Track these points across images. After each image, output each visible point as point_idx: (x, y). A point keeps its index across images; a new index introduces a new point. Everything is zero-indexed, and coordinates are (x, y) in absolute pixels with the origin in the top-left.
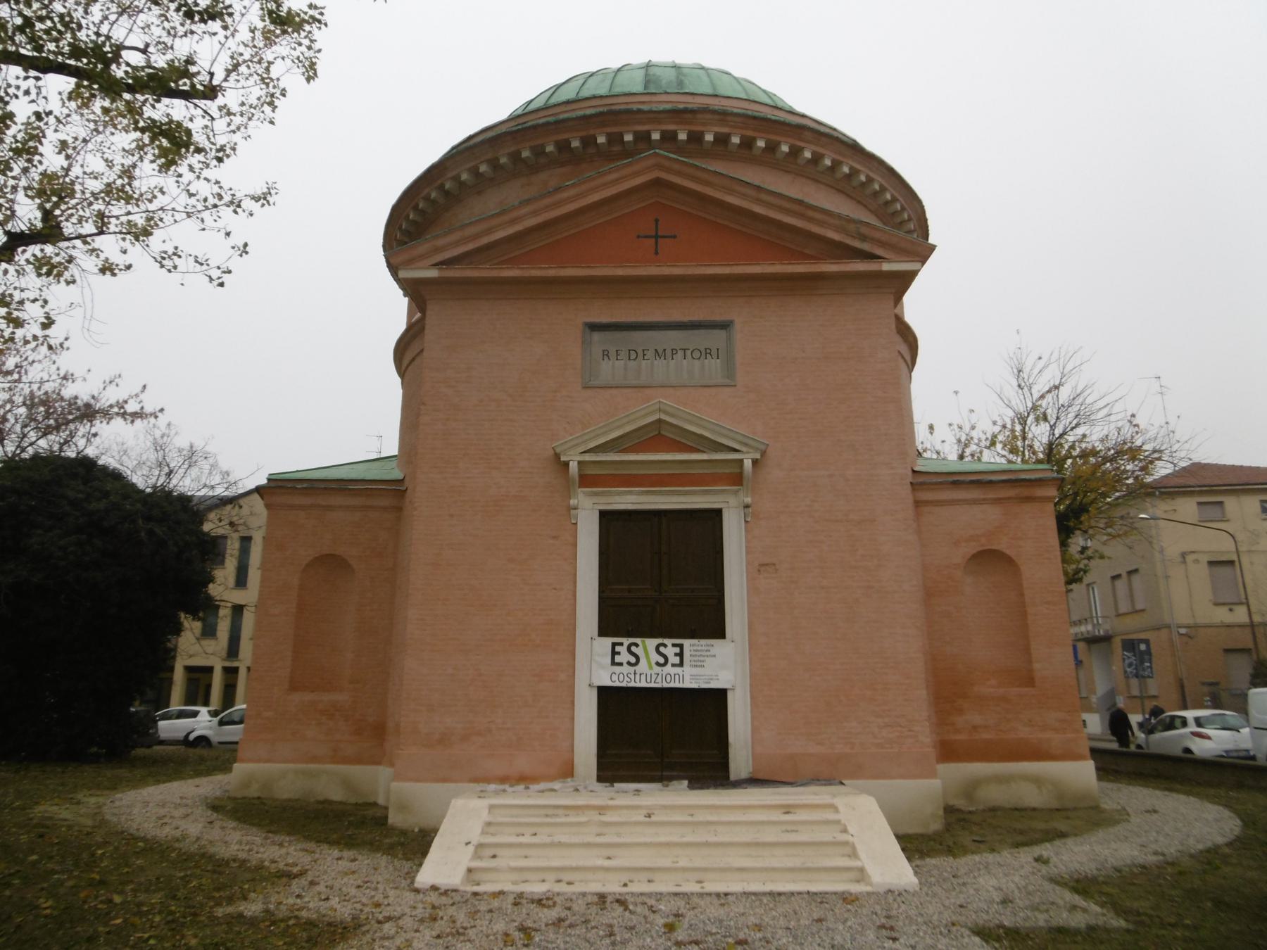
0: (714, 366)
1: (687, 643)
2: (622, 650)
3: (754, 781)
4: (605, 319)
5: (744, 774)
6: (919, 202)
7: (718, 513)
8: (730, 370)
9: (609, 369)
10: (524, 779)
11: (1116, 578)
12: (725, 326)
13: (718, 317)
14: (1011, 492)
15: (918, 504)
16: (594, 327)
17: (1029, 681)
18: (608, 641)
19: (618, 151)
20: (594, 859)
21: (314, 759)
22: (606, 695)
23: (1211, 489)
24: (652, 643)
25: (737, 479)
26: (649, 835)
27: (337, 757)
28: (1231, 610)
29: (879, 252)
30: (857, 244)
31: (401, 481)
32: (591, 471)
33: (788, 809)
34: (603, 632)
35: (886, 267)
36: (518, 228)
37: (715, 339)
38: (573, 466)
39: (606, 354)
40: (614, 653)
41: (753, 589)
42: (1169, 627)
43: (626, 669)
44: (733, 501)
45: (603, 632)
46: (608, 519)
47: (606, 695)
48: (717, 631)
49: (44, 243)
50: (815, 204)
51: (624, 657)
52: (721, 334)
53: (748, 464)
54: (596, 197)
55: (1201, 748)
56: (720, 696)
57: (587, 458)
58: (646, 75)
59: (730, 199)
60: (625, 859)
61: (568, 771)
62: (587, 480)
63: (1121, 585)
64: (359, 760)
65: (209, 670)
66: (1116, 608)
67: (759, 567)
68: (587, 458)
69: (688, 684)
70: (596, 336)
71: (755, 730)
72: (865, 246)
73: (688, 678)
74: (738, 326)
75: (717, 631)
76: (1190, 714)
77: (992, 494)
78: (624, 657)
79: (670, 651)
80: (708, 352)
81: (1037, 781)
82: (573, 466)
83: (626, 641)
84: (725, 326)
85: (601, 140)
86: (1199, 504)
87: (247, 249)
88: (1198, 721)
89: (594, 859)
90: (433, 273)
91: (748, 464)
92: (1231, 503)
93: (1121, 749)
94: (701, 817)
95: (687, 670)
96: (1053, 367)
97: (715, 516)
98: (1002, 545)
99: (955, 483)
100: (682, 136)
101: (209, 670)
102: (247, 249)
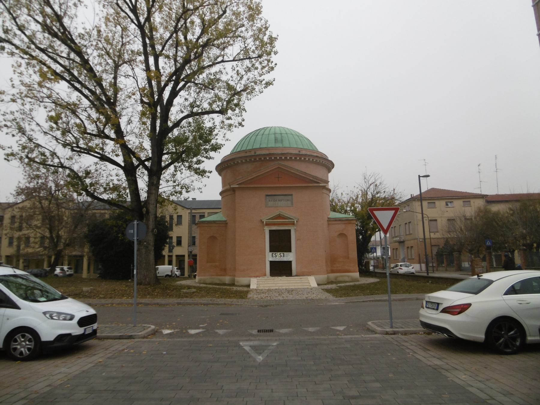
0: (289, 202)
1: (285, 253)
2: (274, 254)
4: (269, 194)
5: (295, 275)
6: (331, 161)
7: (290, 230)
8: (292, 204)
9: (270, 203)
10: (259, 277)
11: (406, 224)
13: (290, 193)
14: (347, 222)
15: (329, 224)
16: (267, 195)
17: (348, 258)
19: (271, 160)
20: (274, 285)
21: (213, 276)
22: (271, 262)
23: (431, 198)
24: (279, 253)
25: (293, 224)
26: (281, 282)
27: (217, 275)
29: (319, 182)
30: (315, 180)
31: (226, 221)
32: (267, 223)
33: (301, 278)
34: (270, 251)
35: (321, 185)
36: (253, 177)
37: (289, 198)
38: (265, 222)
39: (269, 201)
40: (272, 255)
41: (296, 243)
42: (417, 239)
43: (274, 258)
44: (293, 228)
45: (270, 251)
46: (271, 231)
47: (271, 262)
48: (290, 251)
49: (124, 155)
50: (309, 173)
51: (274, 256)
52: (290, 197)
53: (295, 222)
54: (267, 171)
55: (401, 271)
56: (290, 263)
57: (267, 221)
58: (275, 137)
60: (278, 285)
61: (265, 275)
62: (267, 224)
63: (407, 225)
64: (221, 275)
65: (184, 256)
66: (406, 233)
67: (297, 240)
68: (267, 221)
69: (285, 260)
70: (268, 197)
71: (297, 268)
72: (317, 181)
73: (285, 259)
75: (290, 251)
76: (399, 264)
77: (343, 222)
78: (274, 256)
79: (282, 255)
80: (288, 200)
81: (348, 276)
82: (265, 222)
83: (274, 253)
84: (291, 195)
85: (268, 158)
86: (428, 203)
88: (401, 266)
89: (274, 285)
90: (237, 186)
91: (295, 222)
92: (437, 203)
95: (285, 258)
96: (373, 178)
97: (290, 230)
98: (345, 232)
99: (336, 220)
100: (283, 158)
101: (184, 256)
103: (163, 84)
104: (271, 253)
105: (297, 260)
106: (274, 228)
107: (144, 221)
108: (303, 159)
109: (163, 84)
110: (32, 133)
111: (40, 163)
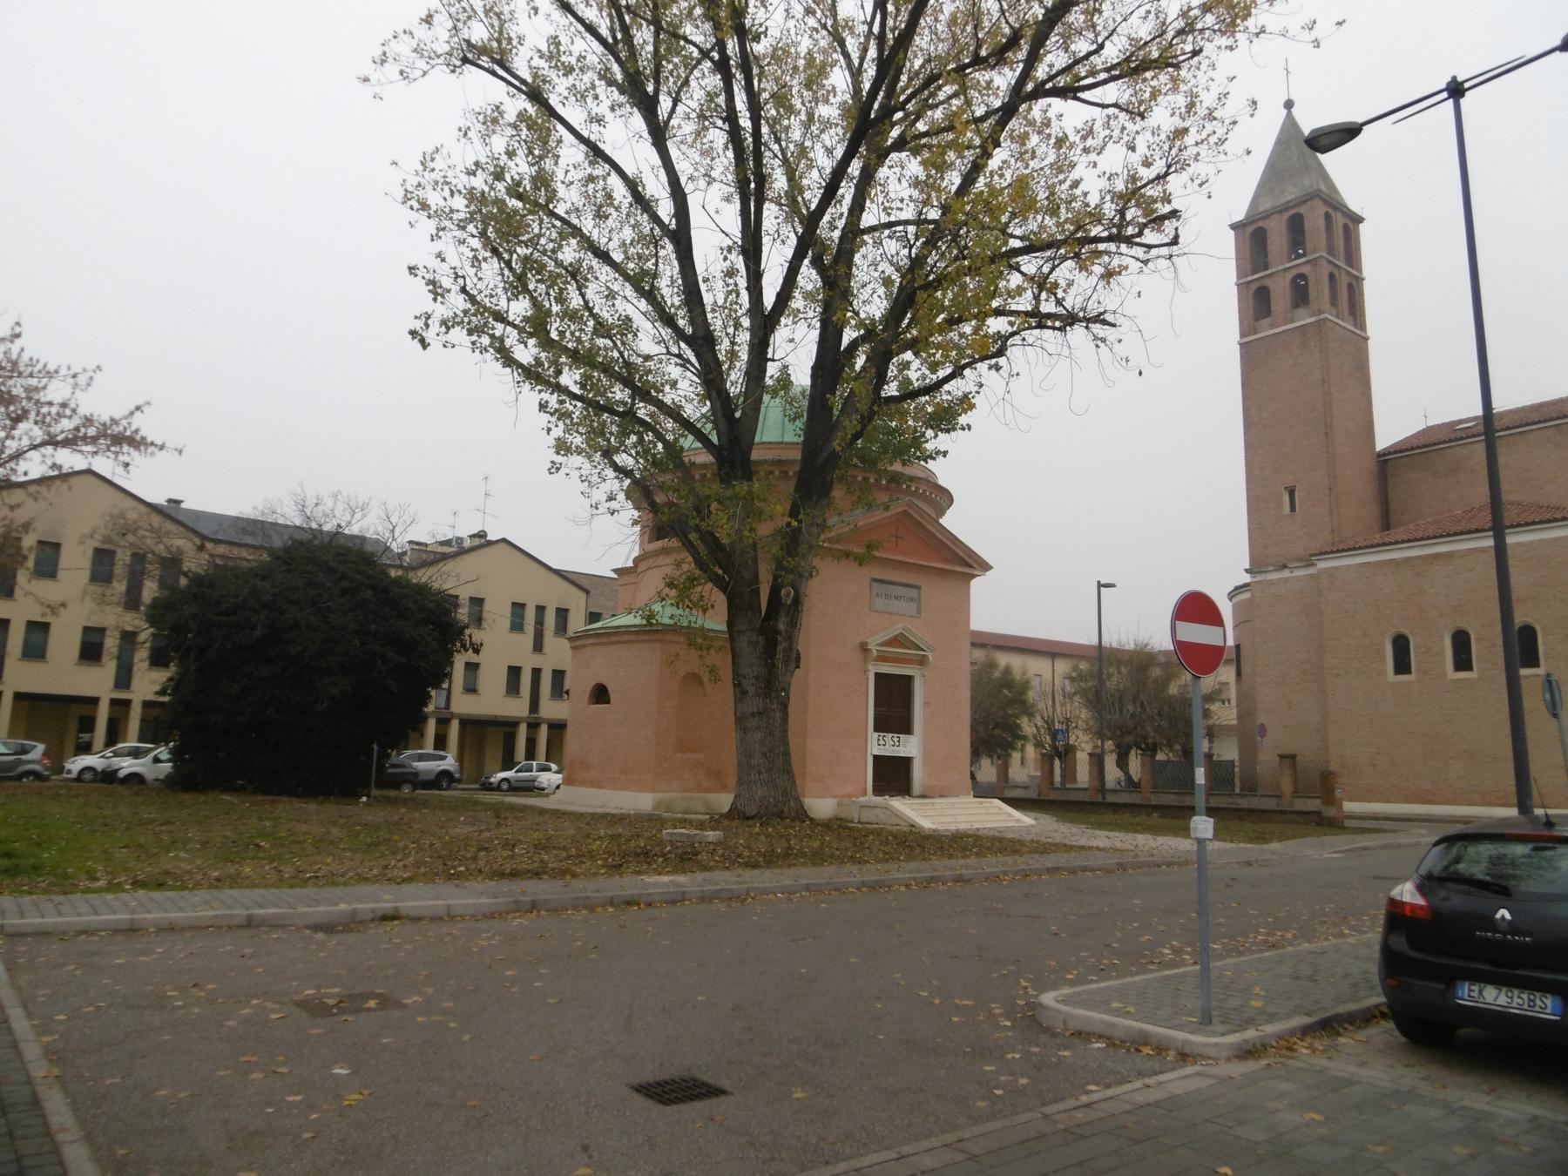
1: (901, 736)
3: (923, 796)
4: (879, 577)
8: (919, 611)
9: (879, 603)
12: (918, 588)
13: (917, 584)
16: (875, 580)
18: (877, 734)
21: (690, 791)
24: (890, 735)
25: (922, 661)
27: (700, 790)
28: (1097, 346)
29: (974, 565)
37: (913, 593)
46: (878, 676)
47: (876, 758)
52: (915, 591)
59: (927, 526)
63: (903, 234)
64: (709, 790)
70: (875, 585)
74: (923, 587)
78: (882, 742)
79: (896, 740)
83: (882, 734)
87: (439, 259)
93: (1411, 953)
94: (957, 806)
95: (901, 749)
102: (439, 259)
103: (856, 62)
104: (877, 734)
105: (926, 753)
106: (886, 669)
107: (90, 587)
108: (913, 489)
109: (856, 62)
110: (1198, 104)
111: (1031, 279)
